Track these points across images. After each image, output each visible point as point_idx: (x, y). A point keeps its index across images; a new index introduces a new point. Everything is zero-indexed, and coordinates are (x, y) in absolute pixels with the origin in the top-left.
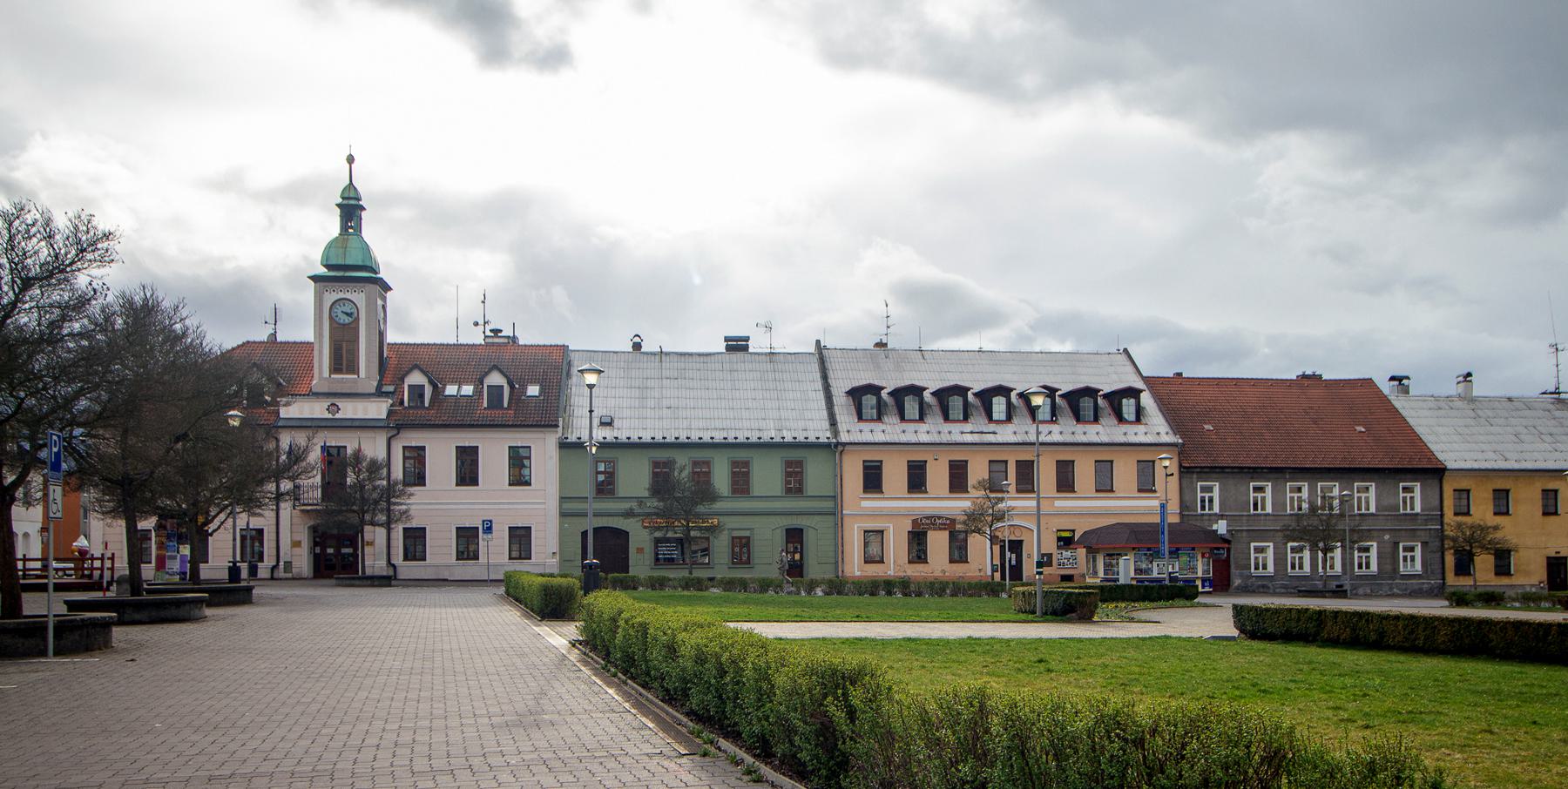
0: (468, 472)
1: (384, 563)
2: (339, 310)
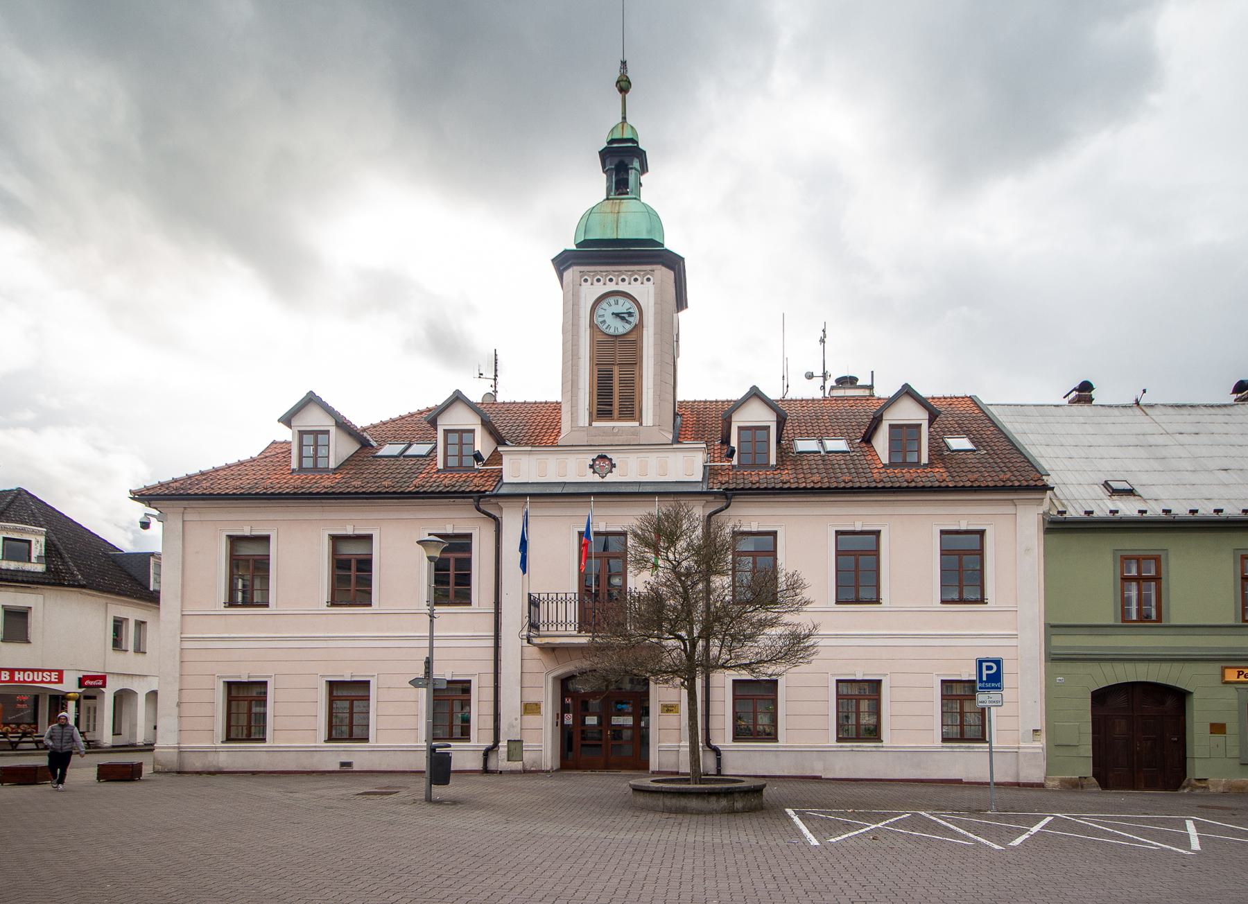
0: (351, 578)
2: (608, 309)
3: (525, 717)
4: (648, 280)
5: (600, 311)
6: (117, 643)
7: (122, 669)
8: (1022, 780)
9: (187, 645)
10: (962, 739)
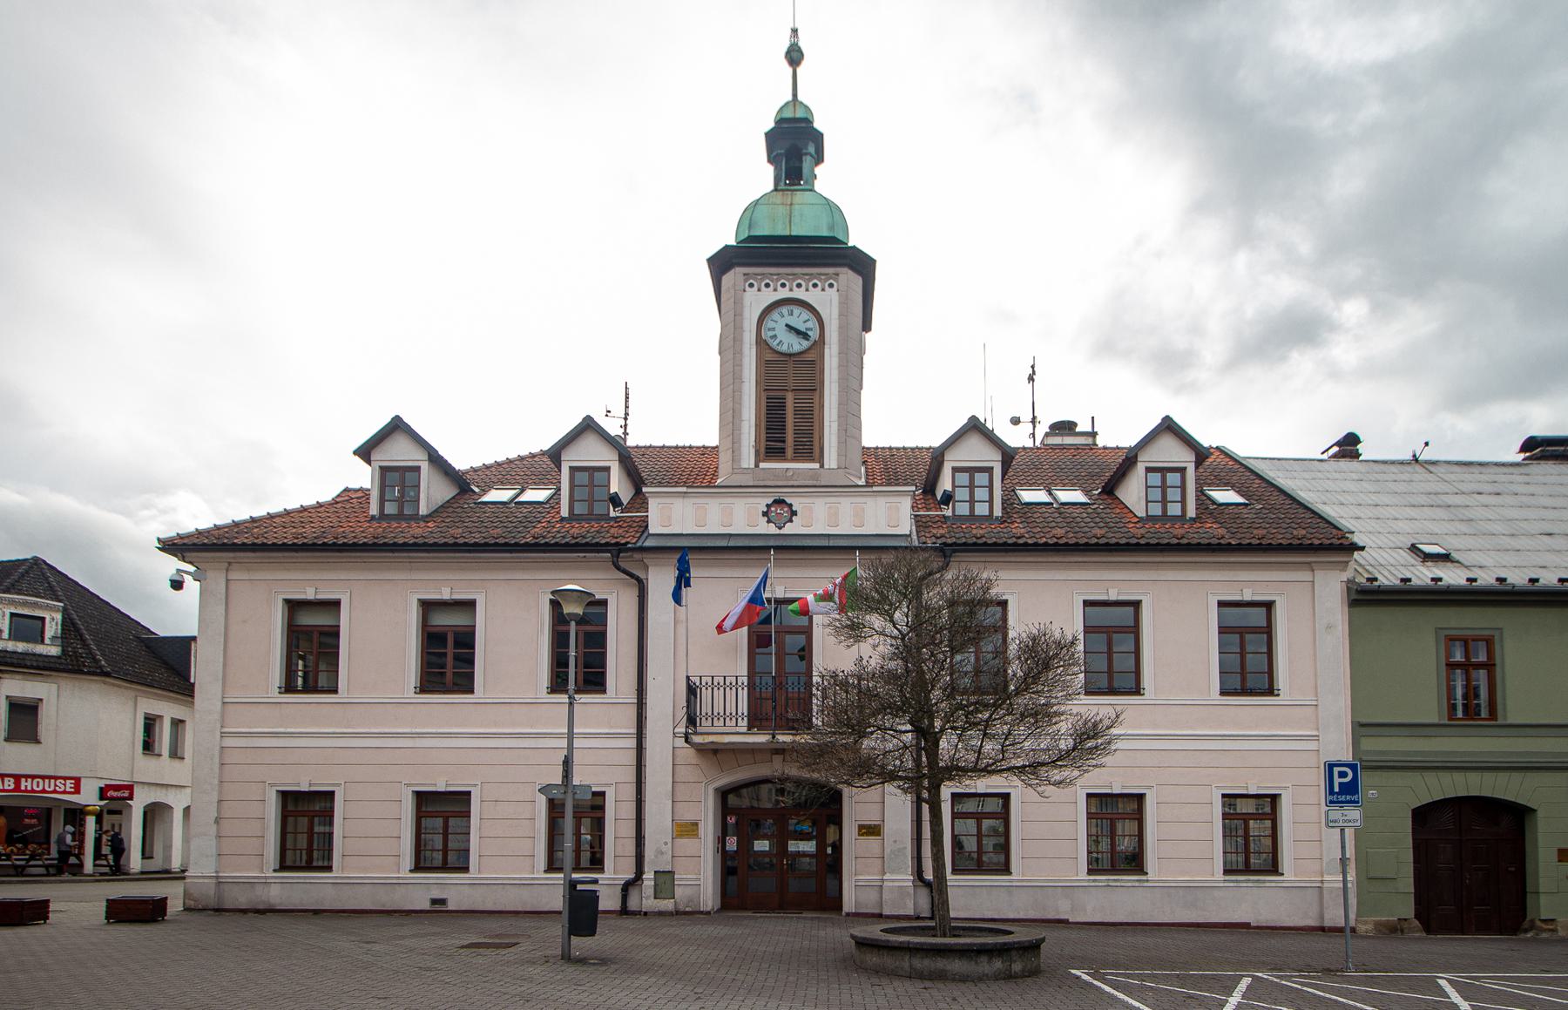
0: (447, 659)
1: (906, 878)
2: (778, 322)
3: (680, 841)
4: (831, 286)
5: (769, 323)
6: (148, 746)
7: (157, 778)
8: (1327, 924)
9: (229, 742)
10: (1247, 870)
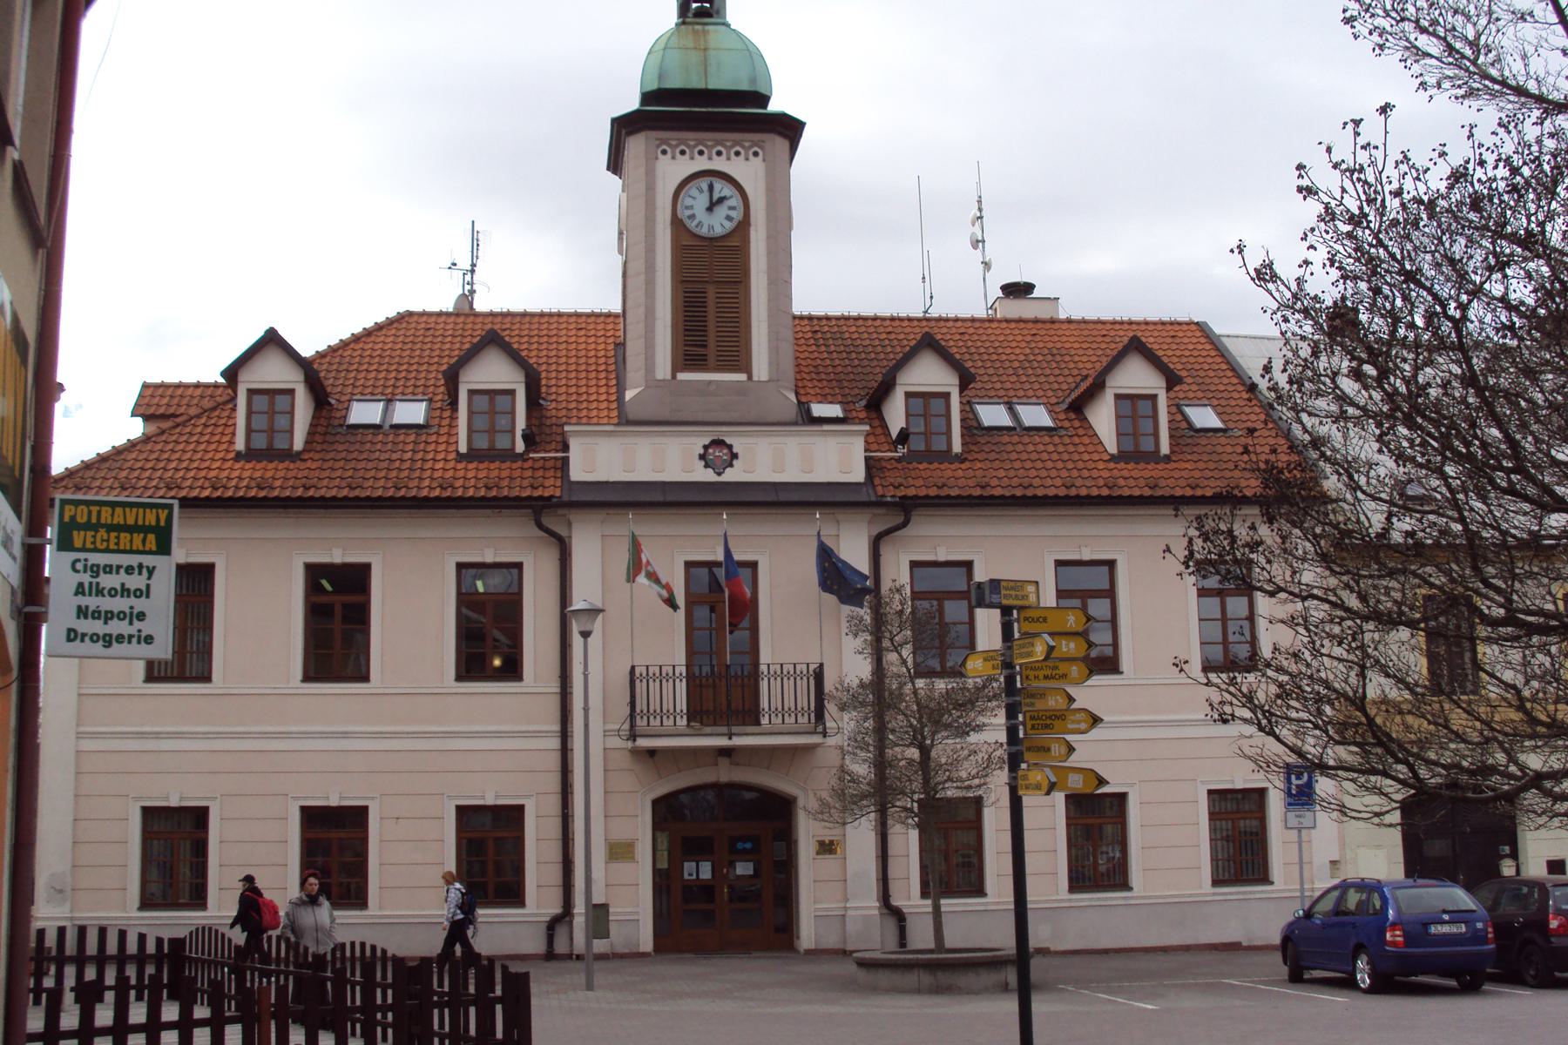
0: (337, 629)
1: (872, 903)
9: (87, 745)
